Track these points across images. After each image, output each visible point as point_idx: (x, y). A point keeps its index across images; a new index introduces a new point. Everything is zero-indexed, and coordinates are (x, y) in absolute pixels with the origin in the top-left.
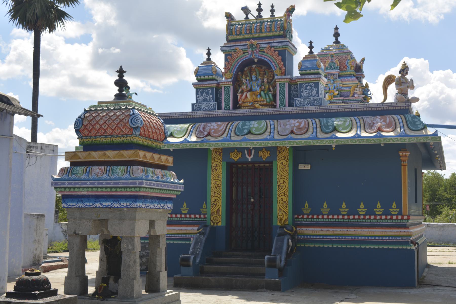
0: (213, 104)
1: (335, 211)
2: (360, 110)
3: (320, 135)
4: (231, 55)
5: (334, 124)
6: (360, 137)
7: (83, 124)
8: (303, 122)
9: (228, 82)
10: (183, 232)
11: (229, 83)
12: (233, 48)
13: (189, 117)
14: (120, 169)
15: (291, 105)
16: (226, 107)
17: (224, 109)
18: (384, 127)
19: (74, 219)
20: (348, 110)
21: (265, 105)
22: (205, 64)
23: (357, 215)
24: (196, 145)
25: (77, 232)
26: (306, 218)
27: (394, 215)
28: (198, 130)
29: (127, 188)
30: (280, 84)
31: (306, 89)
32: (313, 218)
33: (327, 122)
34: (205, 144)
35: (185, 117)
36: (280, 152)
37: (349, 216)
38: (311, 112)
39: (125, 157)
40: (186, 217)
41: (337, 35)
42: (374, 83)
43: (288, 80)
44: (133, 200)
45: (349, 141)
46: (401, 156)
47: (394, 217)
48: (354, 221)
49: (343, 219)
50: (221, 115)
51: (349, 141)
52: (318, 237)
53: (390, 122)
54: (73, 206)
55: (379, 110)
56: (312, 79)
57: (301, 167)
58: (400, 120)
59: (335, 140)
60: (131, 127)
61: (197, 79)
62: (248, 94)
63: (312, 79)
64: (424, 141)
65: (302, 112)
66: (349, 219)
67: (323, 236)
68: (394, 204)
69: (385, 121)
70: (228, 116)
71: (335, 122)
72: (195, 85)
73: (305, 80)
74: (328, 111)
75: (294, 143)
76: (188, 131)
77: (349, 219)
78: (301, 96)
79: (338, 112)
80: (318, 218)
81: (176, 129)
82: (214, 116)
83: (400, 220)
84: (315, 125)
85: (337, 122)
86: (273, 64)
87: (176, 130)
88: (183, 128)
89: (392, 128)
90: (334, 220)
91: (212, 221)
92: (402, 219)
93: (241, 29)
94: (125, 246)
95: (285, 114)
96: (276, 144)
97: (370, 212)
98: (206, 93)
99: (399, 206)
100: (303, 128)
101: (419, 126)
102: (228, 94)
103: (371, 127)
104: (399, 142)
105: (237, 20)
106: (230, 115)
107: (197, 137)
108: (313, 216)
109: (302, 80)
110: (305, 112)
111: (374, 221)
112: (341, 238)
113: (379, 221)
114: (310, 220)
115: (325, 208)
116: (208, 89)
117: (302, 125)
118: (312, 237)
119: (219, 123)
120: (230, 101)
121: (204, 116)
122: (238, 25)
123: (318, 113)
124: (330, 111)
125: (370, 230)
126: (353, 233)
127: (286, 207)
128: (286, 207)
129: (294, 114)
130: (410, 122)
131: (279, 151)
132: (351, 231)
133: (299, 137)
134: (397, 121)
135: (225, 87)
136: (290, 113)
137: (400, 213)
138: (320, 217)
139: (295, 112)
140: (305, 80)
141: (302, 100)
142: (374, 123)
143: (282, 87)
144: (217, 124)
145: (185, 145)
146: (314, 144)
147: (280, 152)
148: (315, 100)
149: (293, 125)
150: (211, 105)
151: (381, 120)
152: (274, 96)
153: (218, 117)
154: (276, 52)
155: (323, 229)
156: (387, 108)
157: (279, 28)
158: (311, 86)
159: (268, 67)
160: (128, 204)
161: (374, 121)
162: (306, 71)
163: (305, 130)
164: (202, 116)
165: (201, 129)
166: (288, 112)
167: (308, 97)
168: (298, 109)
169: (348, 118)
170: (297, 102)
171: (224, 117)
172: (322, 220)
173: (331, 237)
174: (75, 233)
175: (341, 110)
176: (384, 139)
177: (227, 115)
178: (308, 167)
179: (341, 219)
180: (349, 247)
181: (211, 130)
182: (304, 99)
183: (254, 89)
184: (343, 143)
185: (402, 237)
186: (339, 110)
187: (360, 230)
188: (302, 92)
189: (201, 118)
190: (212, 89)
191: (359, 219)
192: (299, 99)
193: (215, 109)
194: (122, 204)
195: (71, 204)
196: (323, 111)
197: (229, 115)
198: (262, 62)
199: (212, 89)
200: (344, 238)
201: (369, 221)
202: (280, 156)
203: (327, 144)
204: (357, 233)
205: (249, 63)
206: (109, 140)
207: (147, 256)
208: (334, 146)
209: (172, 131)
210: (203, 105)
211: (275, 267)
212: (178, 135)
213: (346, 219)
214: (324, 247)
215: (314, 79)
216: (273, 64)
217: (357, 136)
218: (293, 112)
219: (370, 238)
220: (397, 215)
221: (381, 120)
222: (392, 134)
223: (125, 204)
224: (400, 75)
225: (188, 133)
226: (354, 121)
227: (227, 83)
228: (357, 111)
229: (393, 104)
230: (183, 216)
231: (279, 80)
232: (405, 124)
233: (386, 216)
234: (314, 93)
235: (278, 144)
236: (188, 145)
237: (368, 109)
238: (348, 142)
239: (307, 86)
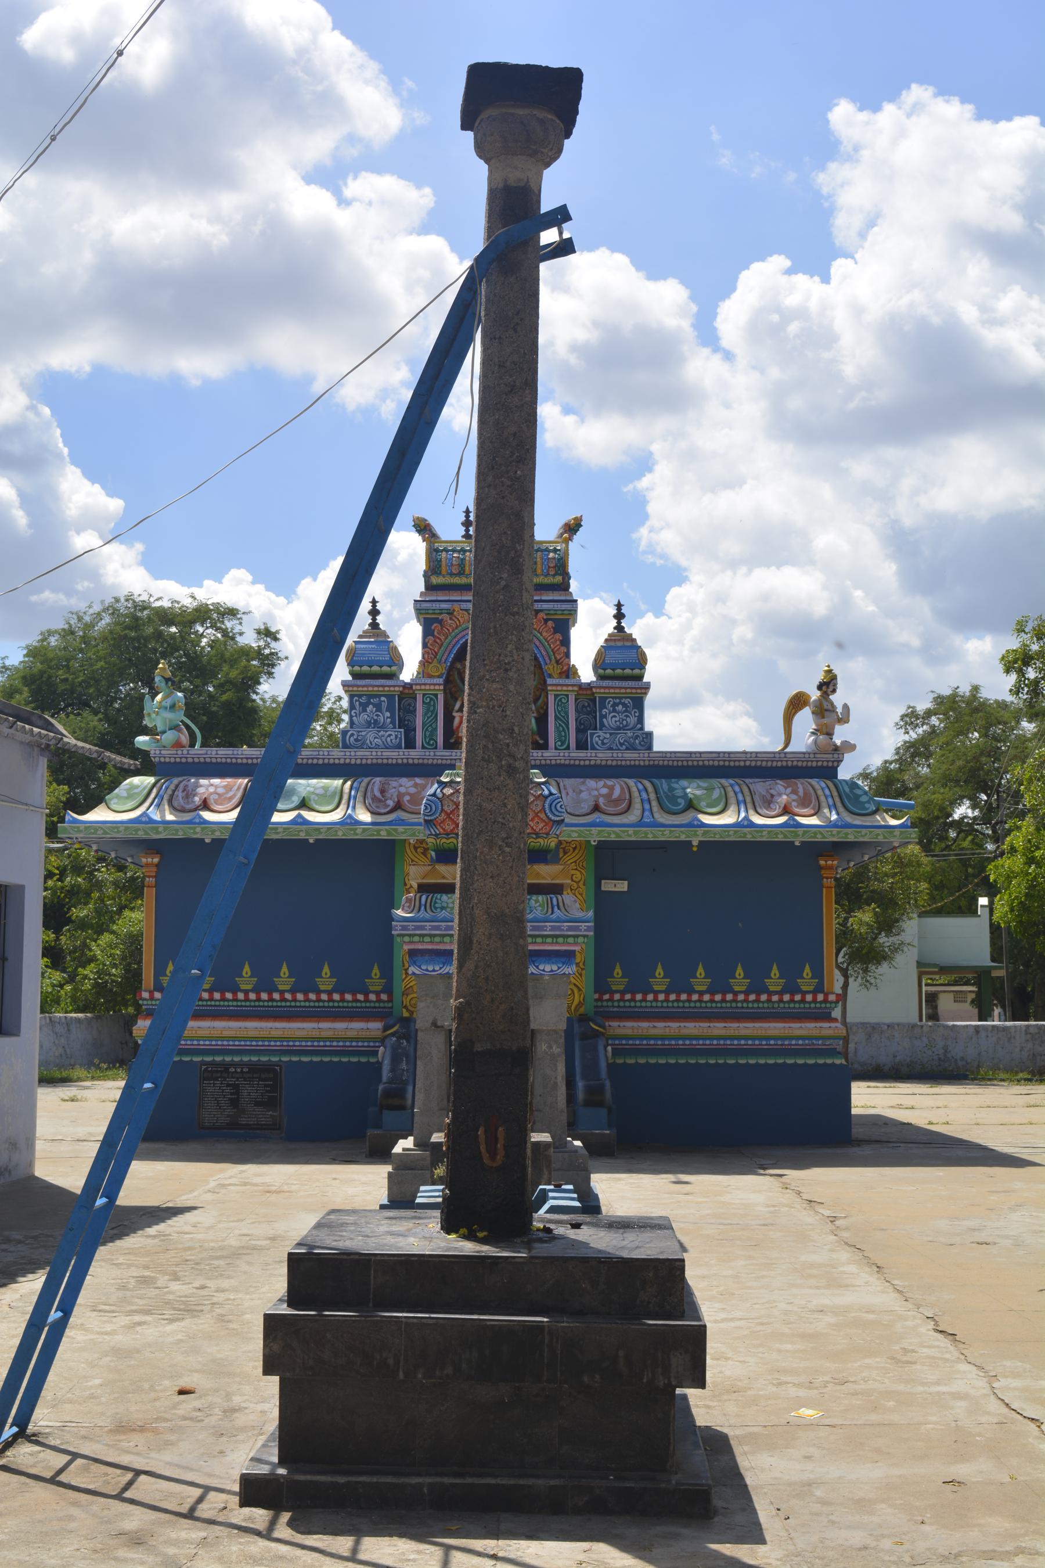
0: (394, 735)
2: (737, 764)
3: (661, 817)
4: (441, 622)
5: (686, 794)
6: (752, 825)
7: (442, 810)
8: (617, 786)
9: (435, 685)
10: (324, 1034)
11: (437, 687)
12: (444, 606)
13: (337, 761)
14: (537, 901)
15: (581, 745)
16: (428, 744)
17: (423, 747)
18: (794, 804)
19: (433, 997)
20: (711, 763)
22: (370, 637)
23: (729, 992)
24: (378, 831)
25: (439, 1023)
26: (618, 1001)
27: (809, 992)
28: (369, 794)
29: (557, 936)
30: (556, 696)
31: (614, 711)
32: (633, 1000)
33: (671, 789)
34: (401, 829)
35: (326, 761)
36: (565, 853)
37: (713, 994)
38: (628, 763)
39: (544, 878)
40: (330, 1000)
43: (576, 688)
44: (563, 960)
45: (731, 833)
46: (821, 868)
47: (809, 997)
48: (724, 1005)
49: (700, 1001)
50: (416, 761)
51: (731, 833)
52: (645, 1042)
53: (805, 793)
54: (434, 971)
55: (777, 767)
56: (629, 691)
57: (608, 886)
58: (827, 792)
59: (700, 831)
60: (550, 819)
61: (352, 673)
63: (629, 691)
64: (885, 838)
65: (609, 763)
66: (712, 1001)
67: (656, 1038)
68: (807, 969)
69: (795, 792)
70: (432, 764)
71: (688, 790)
72: (348, 686)
73: (612, 691)
74: (666, 763)
75: (609, 834)
76: (345, 797)
77: (712, 1001)
78: (602, 725)
79: (688, 766)
80: (644, 1000)
81: (312, 789)
82: (400, 761)
83: (821, 1002)
84: (644, 795)
85: (693, 789)
86: (541, 649)
87: (313, 793)
88: (331, 789)
89: (813, 808)
90: (681, 1004)
91: (406, 1007)
92: (826, 1001)
93: (462, 563)
94: (544, 1047)
95: (569, 765)
96: (570, 836)
97: (757, 987)
98: (374, 705)
99: (818, 973)
100: (617, 802)
101: (867, 805)
102: (432, 712)
103: (768, 802)
104: (835, 839)
105: (443, 538)
106: (440, 762)
107: (372, 813)
108: (633, 994)
109: (607, 691)
110: (614, 763)
111: (766, 1005)
112: (694, 1042)
113: (776, 1005)
114: (627, 1004)
115: (660, 978)
116: (380, 696)
117: (617, 793)
118: (631, 1042)
119: (418, 780)
120: (436, 729)
121: (375, 761)
122: (454, 551)
123: (645, 766)
124: (671, 763)
125: (757, 1025)
126: (722, 1032)
127: (581, 975)
128: (581, 975)
129: (590, 765)
130: (847, 796)
131: (564, 849)
132: (718, 1028)
133: (616, 820)
134: (820, 792)
135: (424, 695)
136: (582, 763)
137: (819, 989)
138: (650, 997)
139: (593, 763)
140: (612, 691)
141: (608, 736)
142: (772, 796)
143: (561, 704)
144: (411, 783)
145: (351, 830)
146: (655, 836)
147: (565, 853)
148: (637, 737)
149: (596, 793)
150: (390, 735)
151: (786, 788)
152: (542, 720)
153: (408, 764)
154: (550, 624)
155: (656, 1024)
156: (795, 763)
157: (554, 567)
158: (624, 705)
160: (555, 968)
161: (772, 792)
162: (613, 670)
163: (625, 805)
164: (369, 762)
165: (378, 794)
166: (577, 762)
167: (619, 728)
168: (599, 755)
169: (715, 782)
170: (595, 739)
171: (423, 765)
172: (654, 1004)
173: (673, 1042)
174: (434, 1024)
175: (695, 763)
176: (805, 832)
177: (430, 762)
178: (623, 886)
179: (695, 1002)
180: (712, 1061)
181: (400, 795)
182: (611, 734)
184: (717, 838)
185: (824, 1038)
186: (690, 763)
187: (737, 1025)
188: (605, 716)
189: (367, 764)
190: (390, 697)
191: (735, 1000)
192: (600, 733)
193: (399, 747)
194: (541, 967)
195: (430, 968)
196: (656, 763)
197: (435, 762)
199: (390, 697)
200: (701, 1042)
201: (756, 1005)
203: (683, 838)
204: (731, 1033)
207: (232, 1094)
208: (695, 843)
209: (303, 795)
210: (370, 735)
211: (600, 1104)
212: (321, 805)
213: (706, 1002)
214: (657, 1064)
215: (634, 691)
216: (541, 649)
217: (746, 823)
218: (587, 763)
219: (757, 1042)
220: (815, 993)
221: (786, 788)
222: (814, 821)
223: (548, 968)
224: (819, 693)
225: (344, 801)
226: (729, 789)
227: (432, 687)
228: (729, 766)
229: (807, 756)
230: (324, 997)
231: (554, 688)
232: (837, 799)
233: (792, 995)
234: (632, 720)
235: (575, 835)
236: (359, 831)
237: (753, 764)
238: (729, 836)
239: (617, 705)
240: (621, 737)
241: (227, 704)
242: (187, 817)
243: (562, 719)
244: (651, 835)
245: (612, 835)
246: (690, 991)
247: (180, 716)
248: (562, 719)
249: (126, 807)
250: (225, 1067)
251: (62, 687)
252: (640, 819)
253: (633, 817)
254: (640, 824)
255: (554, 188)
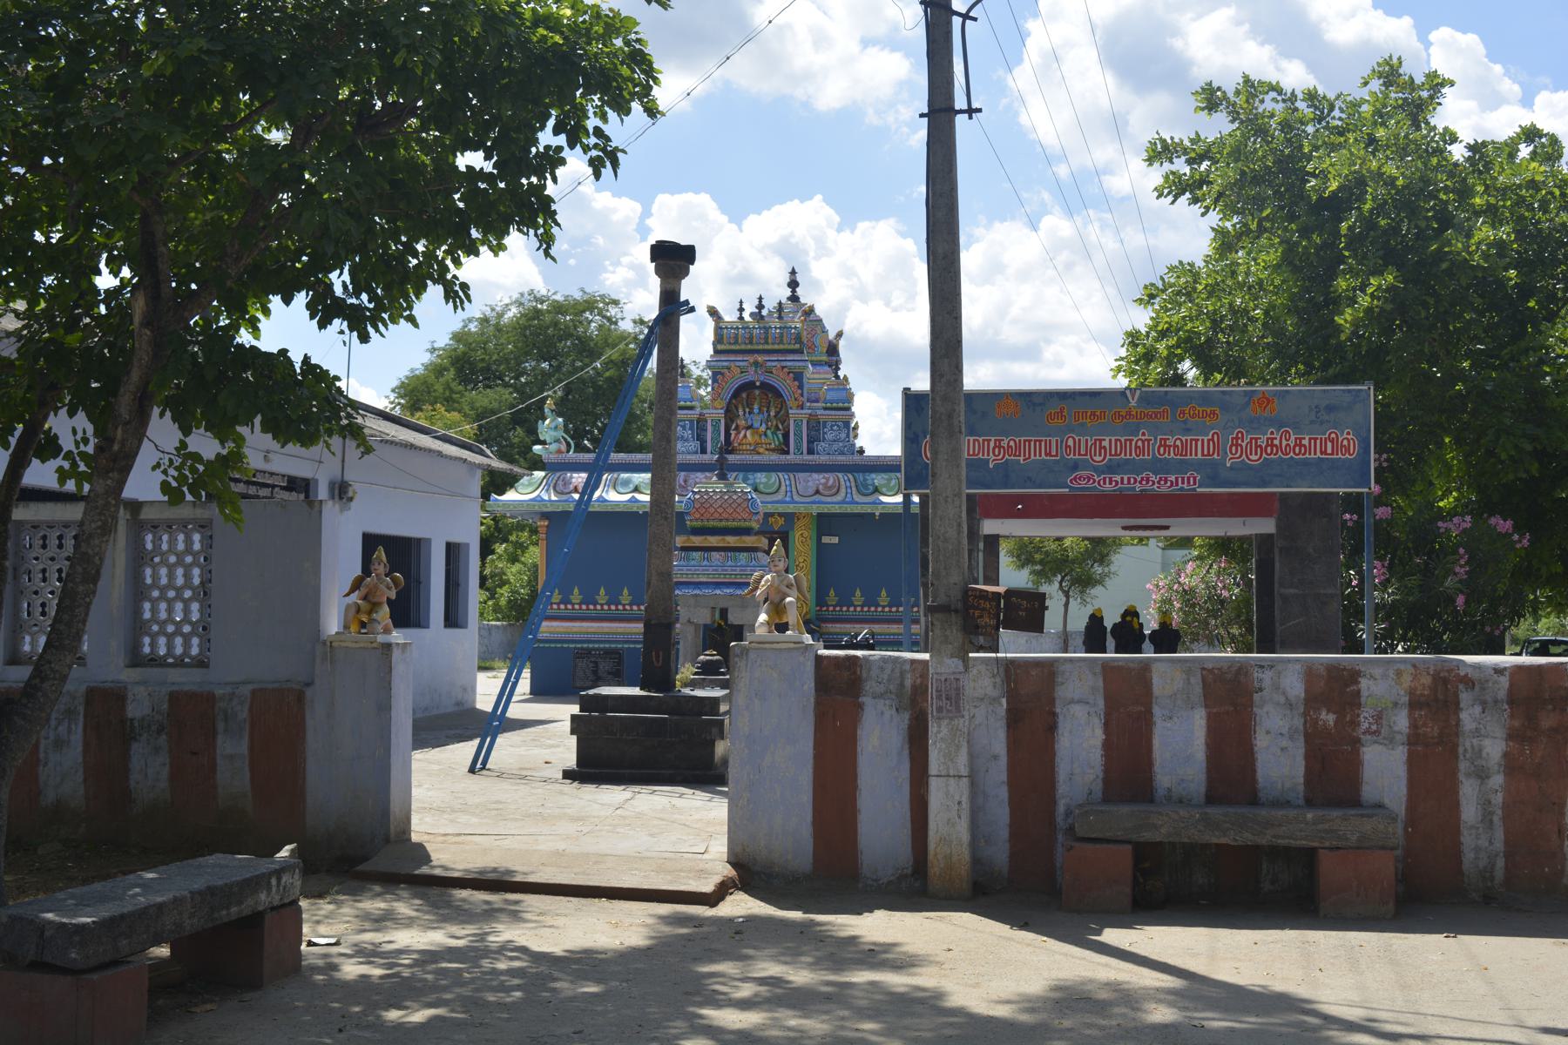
1: (871, 601)
3: (857, 498)
8: (831, 478)
15: (810, 452)
21: (773, 450)
41: (793, 284)
42: (692, 260)
57: (826, 540)
62: (749, 433)
100: (830, 488)
115: (858, 597)
133: (829, 499)
152: (786, 436)
159: (778, 394)
169: (893, 475)
178: (835, 540)
183: (756, 425)
190: (691, 421)
198: (766, 387)
199: (691, 421)
202: (799, 524)
205: (748, 387)
206: (723, 524)
234: (843, 436)
240: (835, 447)
241: (609, 379)
242: (564, 497)
243: (798, 435)
244: (850, 509)
245: (825, 509)
246: (877, 605)
247: (561, 433)
248: (798, 435)
249: (528, 492)
250: (589, 651)
251: (481, 365)
252: (844, 498)
253: (839, 498)
254: (843, 502)
255: (687, 290)
